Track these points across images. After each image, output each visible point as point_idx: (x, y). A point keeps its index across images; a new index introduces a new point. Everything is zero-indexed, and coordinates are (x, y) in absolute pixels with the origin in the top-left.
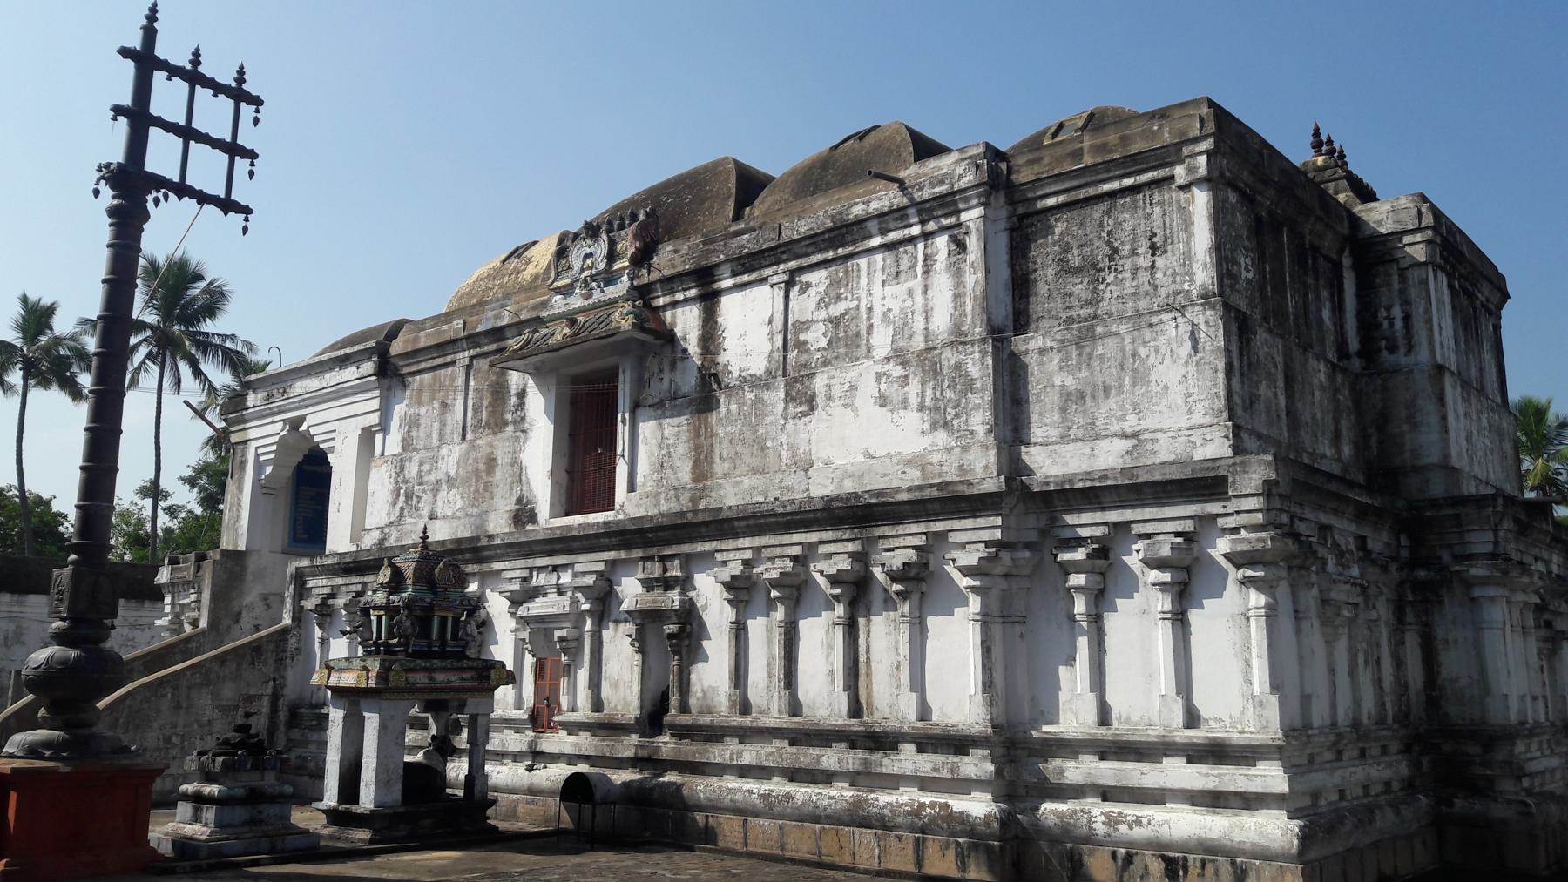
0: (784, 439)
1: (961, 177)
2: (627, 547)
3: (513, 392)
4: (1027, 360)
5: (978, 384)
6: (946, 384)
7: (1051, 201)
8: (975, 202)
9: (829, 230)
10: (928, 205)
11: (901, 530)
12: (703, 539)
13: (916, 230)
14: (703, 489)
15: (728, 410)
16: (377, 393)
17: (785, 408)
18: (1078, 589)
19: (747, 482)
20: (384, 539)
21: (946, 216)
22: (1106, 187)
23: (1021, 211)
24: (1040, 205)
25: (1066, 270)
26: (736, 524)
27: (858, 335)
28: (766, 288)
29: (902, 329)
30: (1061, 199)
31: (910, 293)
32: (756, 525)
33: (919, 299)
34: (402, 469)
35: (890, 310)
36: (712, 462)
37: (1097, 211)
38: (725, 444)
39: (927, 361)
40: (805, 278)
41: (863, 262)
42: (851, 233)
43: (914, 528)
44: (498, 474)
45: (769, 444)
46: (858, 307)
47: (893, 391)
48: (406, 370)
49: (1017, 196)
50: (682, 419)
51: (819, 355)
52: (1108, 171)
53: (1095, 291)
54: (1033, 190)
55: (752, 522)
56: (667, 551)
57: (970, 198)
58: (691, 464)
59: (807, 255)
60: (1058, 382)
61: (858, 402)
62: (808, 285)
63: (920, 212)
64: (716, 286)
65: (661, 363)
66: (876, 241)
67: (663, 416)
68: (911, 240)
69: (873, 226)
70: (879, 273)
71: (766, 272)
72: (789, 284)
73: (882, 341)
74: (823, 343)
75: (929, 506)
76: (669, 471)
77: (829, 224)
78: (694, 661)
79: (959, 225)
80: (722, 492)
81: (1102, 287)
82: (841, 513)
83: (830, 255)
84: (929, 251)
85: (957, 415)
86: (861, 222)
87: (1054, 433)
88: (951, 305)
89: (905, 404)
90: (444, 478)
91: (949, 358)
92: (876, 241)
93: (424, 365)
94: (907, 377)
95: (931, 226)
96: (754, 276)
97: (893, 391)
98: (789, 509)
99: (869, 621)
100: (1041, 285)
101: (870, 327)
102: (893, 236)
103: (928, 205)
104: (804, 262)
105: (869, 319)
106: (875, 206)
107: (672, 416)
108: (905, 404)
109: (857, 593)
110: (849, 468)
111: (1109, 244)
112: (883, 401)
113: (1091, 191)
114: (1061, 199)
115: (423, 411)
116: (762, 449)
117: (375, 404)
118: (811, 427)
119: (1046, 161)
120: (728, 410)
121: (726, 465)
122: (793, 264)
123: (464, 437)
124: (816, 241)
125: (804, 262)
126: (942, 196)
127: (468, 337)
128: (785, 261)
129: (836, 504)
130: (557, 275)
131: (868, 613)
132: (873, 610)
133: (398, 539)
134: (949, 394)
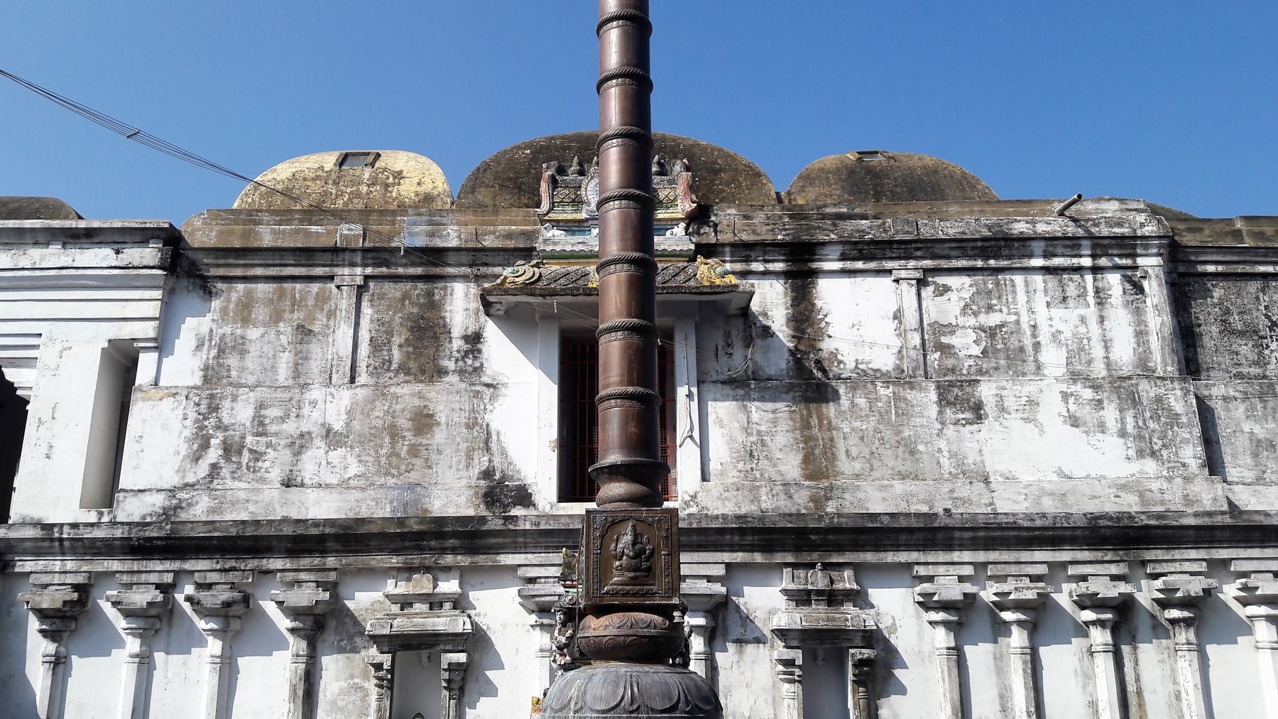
0: (942, 444)
1: (1142, 225)
2: (767, 548)
3: (457, 332)
4: (1212, 404)
5: (1184, 419)
6: (1148, 415)
7: (1211, 268)
8: (1155, 251)
9: (984, 239)
10: (1106, 242)
11: (1177, 554)
12: (897, 548)
13: (1087, 262)
14: (831, 488)
15: (853, 404)
16: (158, 294)
17: (940, 412)
18: (693, 629)
19: (899, 487)
20: (178, 507)
21: (1120, 256)
22: (1262, 269)
23: (1182, 269)
24: (1200, 268)
25: (1227, 330)
26: (957, 534)
27: (1022, 349)
28: (886, 282)
29: (1078, 351)
30: (1220, 268)
31: (1083, 320)
32: (986, 538)
33: (1095, 329)
34: (214, 409)
35: (1060, 332)
36: (834, 457)
37: (1253, 286)
38: (853, 440)
39: (1121, 387)
40: (942, 280)
41: (1019, 279)
42: (1010, 248)
43: (1193, 554)
44: (439, 436)
45: (921, 448)
46: (1018, 322)
47: (1085, 413)
48: (214, 272)
49: (1179, 256)
50: (780, 405)
51: (971, 362)
52: (1266, 256)
53: (1260, 353)
54: (1197, 254)
55: (981, 534)
56: (836, 559)
57: (1152, 246)
58: (800, 457)
59: (948, 258)
60: (1247, 429)
61: (1041, 417)
62: (946, 289)
63: (1094, 247)
64: (815, 265)
65: (728, 335)
66: (1038, 262)
67: (747, 397)
68: (1078, 270)
69: (1038, 246)
70: (1040, 294)
71: (889, 265)
72: (921, 283)
73: (1053, 359)
74: (976, 351)
75: (1218, 533)
76: (764, 464)
77: (986, 233)
78: (885, 693)
79: (1136, 268)
80: (861, 495)
81: (1267, 352)
82: (1108, 532)
83: (979, 263)
84: (1100, 285)
85: (1164, 445)
86: (1024, 240)
87: (1250, 475)
88: (1133, 340)
89: (1102, 427)
90: (315, 430)
91: (1147, 390)
92: (1038, 262)
93: (259, 271)
94: (1100, 402)
95: (1103, 262)
96: (872, 265)
97: (1085, 413)
98: (1038, 523)
99: (1135, 648)
100: (1206, 339)
101: (1037, 346)
102: (1057, 261)
103: (1106, 242)
104: (944, 264)
105: (1034, 336)
106: (1041, 228)
107: (762, 399)
108: (1102, 427)
109: (1123, 619)
110: (1047, 486)
111: (1267, 316)
112: (1074, 422)
113: (1248, 269)
114: (1220, 268)
115: (253, 333)
116: (912, 453)
117: (153, 309)
118: (981, 436)
119: (1207, 232)
120: (853, 404)
121: (857, 466)
122: (928, 263)
123: (352, 380)
124: (961, 246)
125: (944, 264)
126: (1123, 237)
127: (365, 251)
128: (916, 258)
129: (1102, 523)
130: (553, 205)
131: (1133, 640)
132: (1139, 637)
133: (212, 510)
134: (1152, 425)
